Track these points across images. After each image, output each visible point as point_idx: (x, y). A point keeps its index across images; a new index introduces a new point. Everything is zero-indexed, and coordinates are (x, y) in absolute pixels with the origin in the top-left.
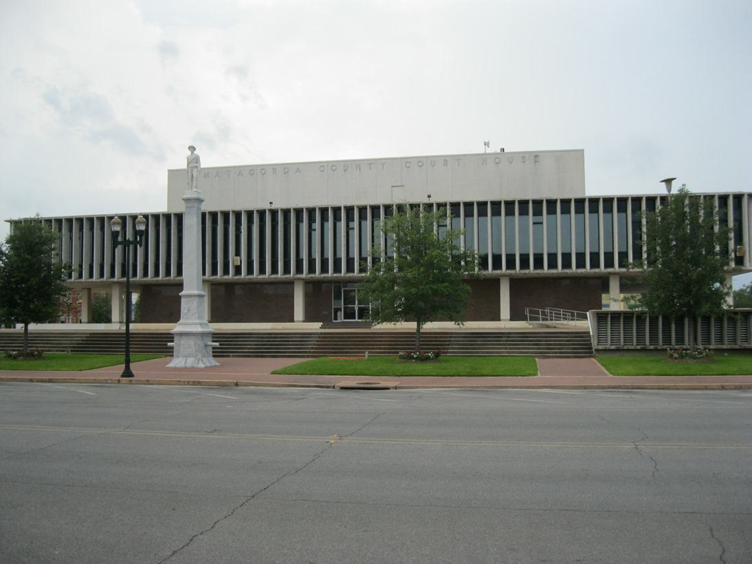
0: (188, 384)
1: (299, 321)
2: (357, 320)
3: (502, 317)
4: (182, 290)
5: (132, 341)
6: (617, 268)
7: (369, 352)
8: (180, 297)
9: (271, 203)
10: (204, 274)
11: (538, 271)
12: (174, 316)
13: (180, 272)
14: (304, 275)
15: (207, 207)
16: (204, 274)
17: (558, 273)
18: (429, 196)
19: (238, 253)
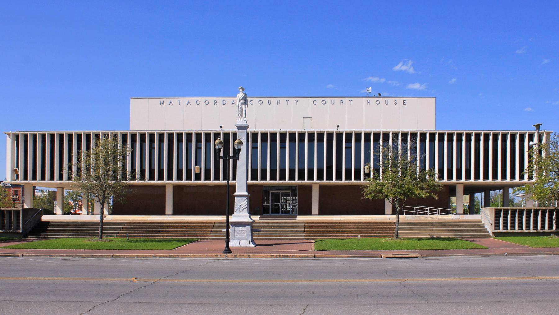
0: (279, 257)
1: (316, 215)
2: (280, 214)
3: (386, 212)
4: (235, 191)
5: (105, 228)
6: (315, 181)
7: (361, 236)
8: (234, 196)
9: (221, 127)
10: (247, 179)
11: (329, 182)
12: (230, 211)
13: (234, 178)
14: (174, 181)
15: (251, 130)
16: (247, 179)
17: (352, 183)
18: (338, 126)
19: (198, 163)
